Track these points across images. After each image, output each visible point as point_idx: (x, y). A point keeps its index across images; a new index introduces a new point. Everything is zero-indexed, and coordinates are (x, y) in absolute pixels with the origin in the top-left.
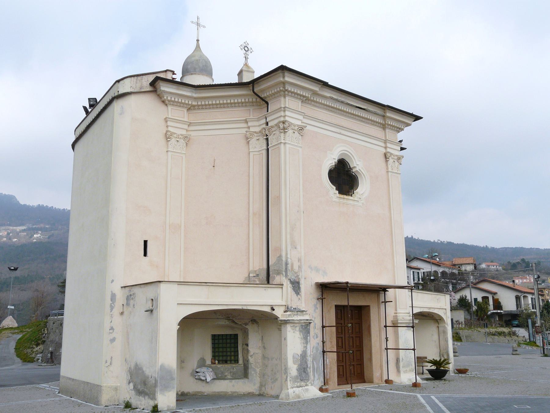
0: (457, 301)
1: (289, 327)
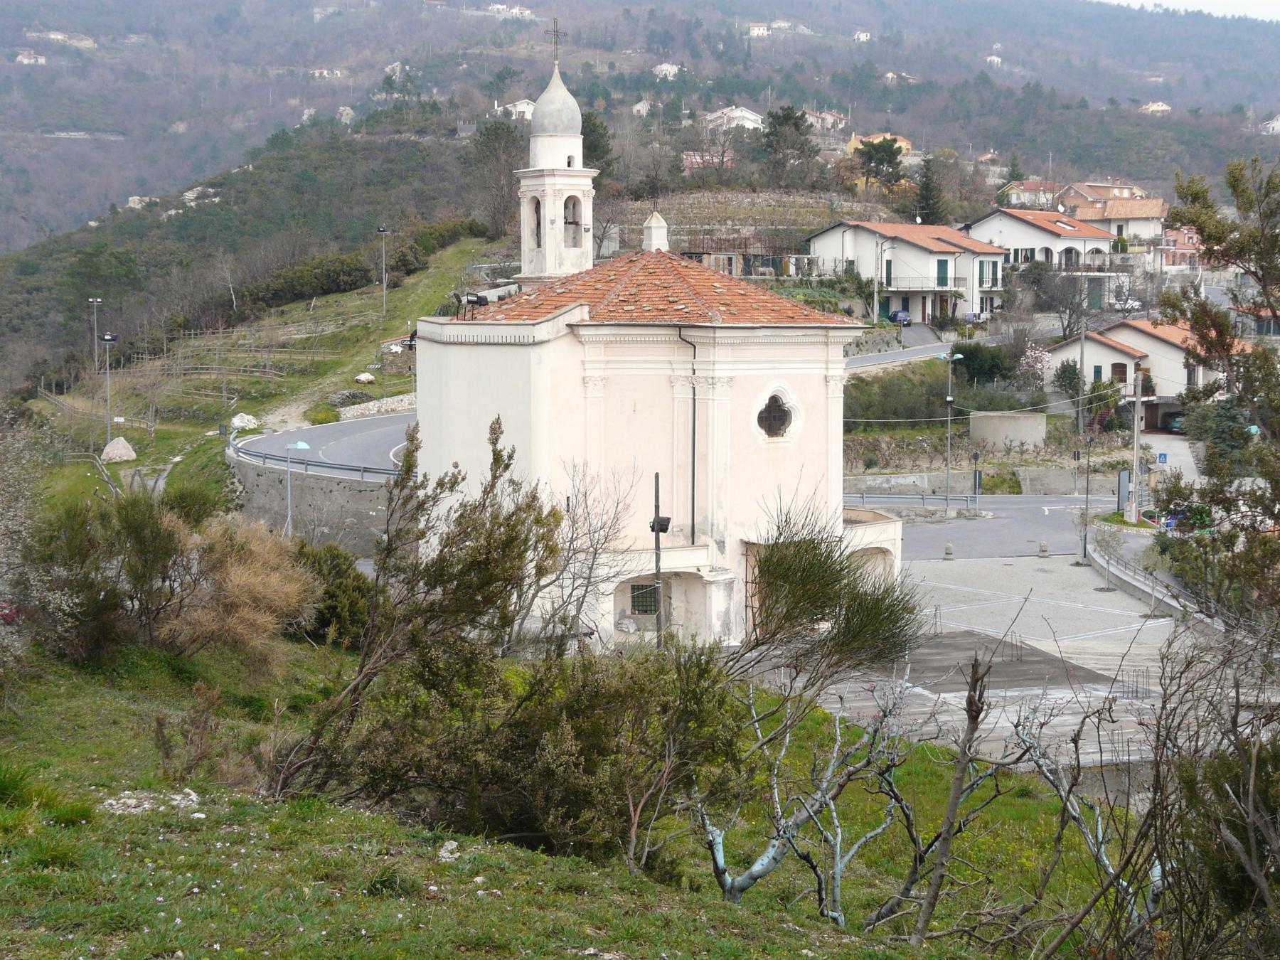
0: (1053, 372)
1: (713, 586)
